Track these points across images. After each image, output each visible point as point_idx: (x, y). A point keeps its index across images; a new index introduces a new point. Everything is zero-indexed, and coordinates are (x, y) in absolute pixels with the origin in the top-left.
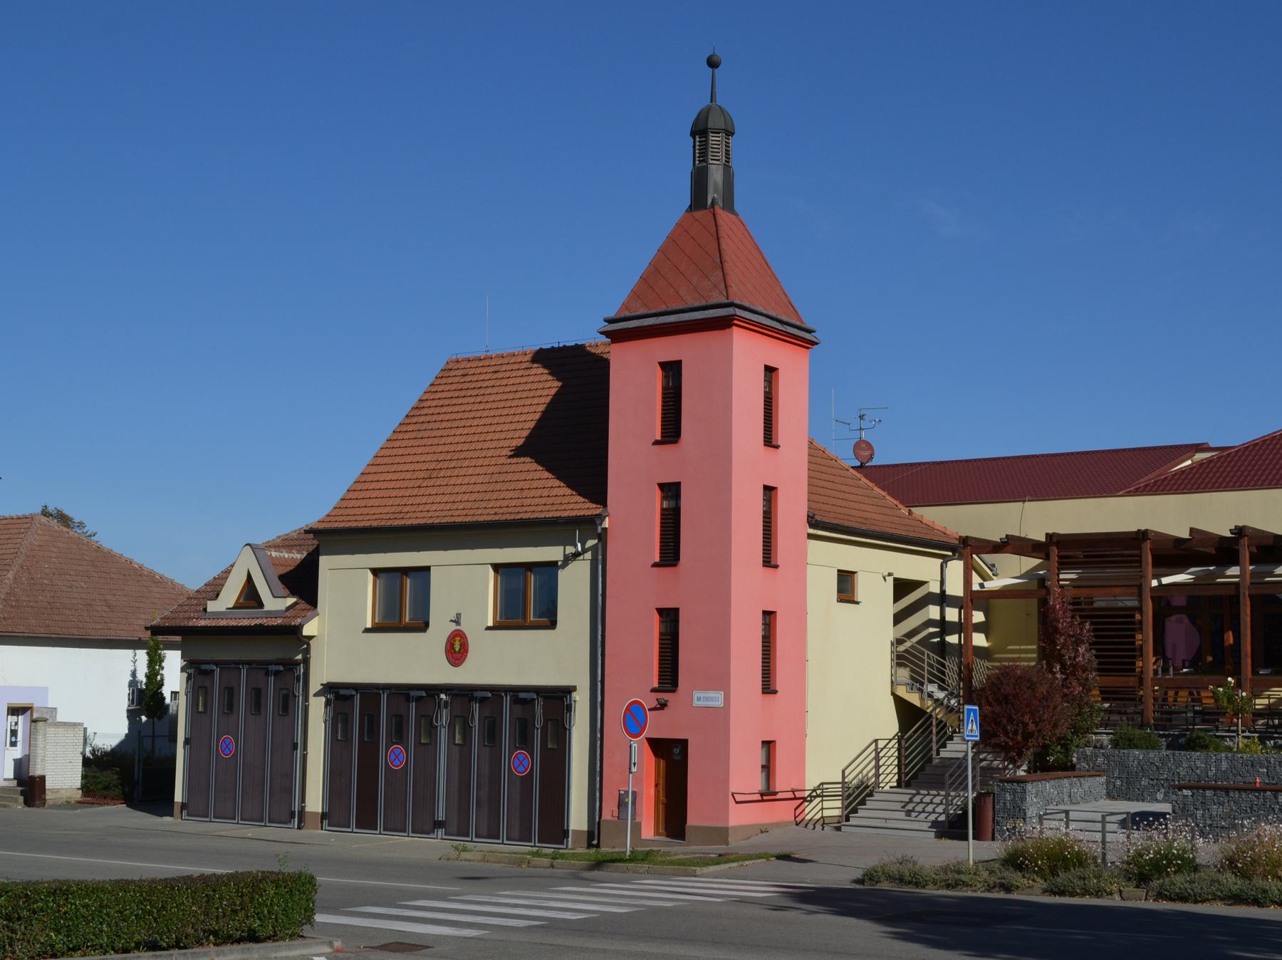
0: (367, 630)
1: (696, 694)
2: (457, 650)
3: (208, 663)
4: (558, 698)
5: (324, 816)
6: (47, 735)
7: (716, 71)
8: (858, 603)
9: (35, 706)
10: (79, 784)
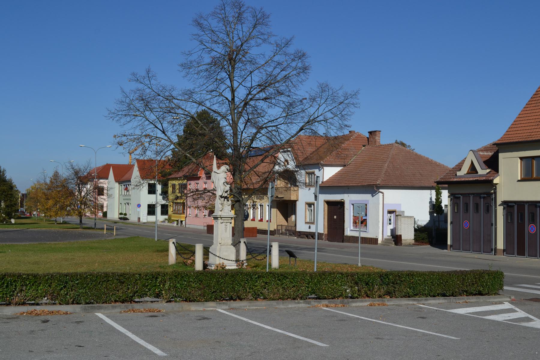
0: (519, 181)
3: (458, 194)
5: (504, 250)
9: (397, 210)
10: (413, 238)
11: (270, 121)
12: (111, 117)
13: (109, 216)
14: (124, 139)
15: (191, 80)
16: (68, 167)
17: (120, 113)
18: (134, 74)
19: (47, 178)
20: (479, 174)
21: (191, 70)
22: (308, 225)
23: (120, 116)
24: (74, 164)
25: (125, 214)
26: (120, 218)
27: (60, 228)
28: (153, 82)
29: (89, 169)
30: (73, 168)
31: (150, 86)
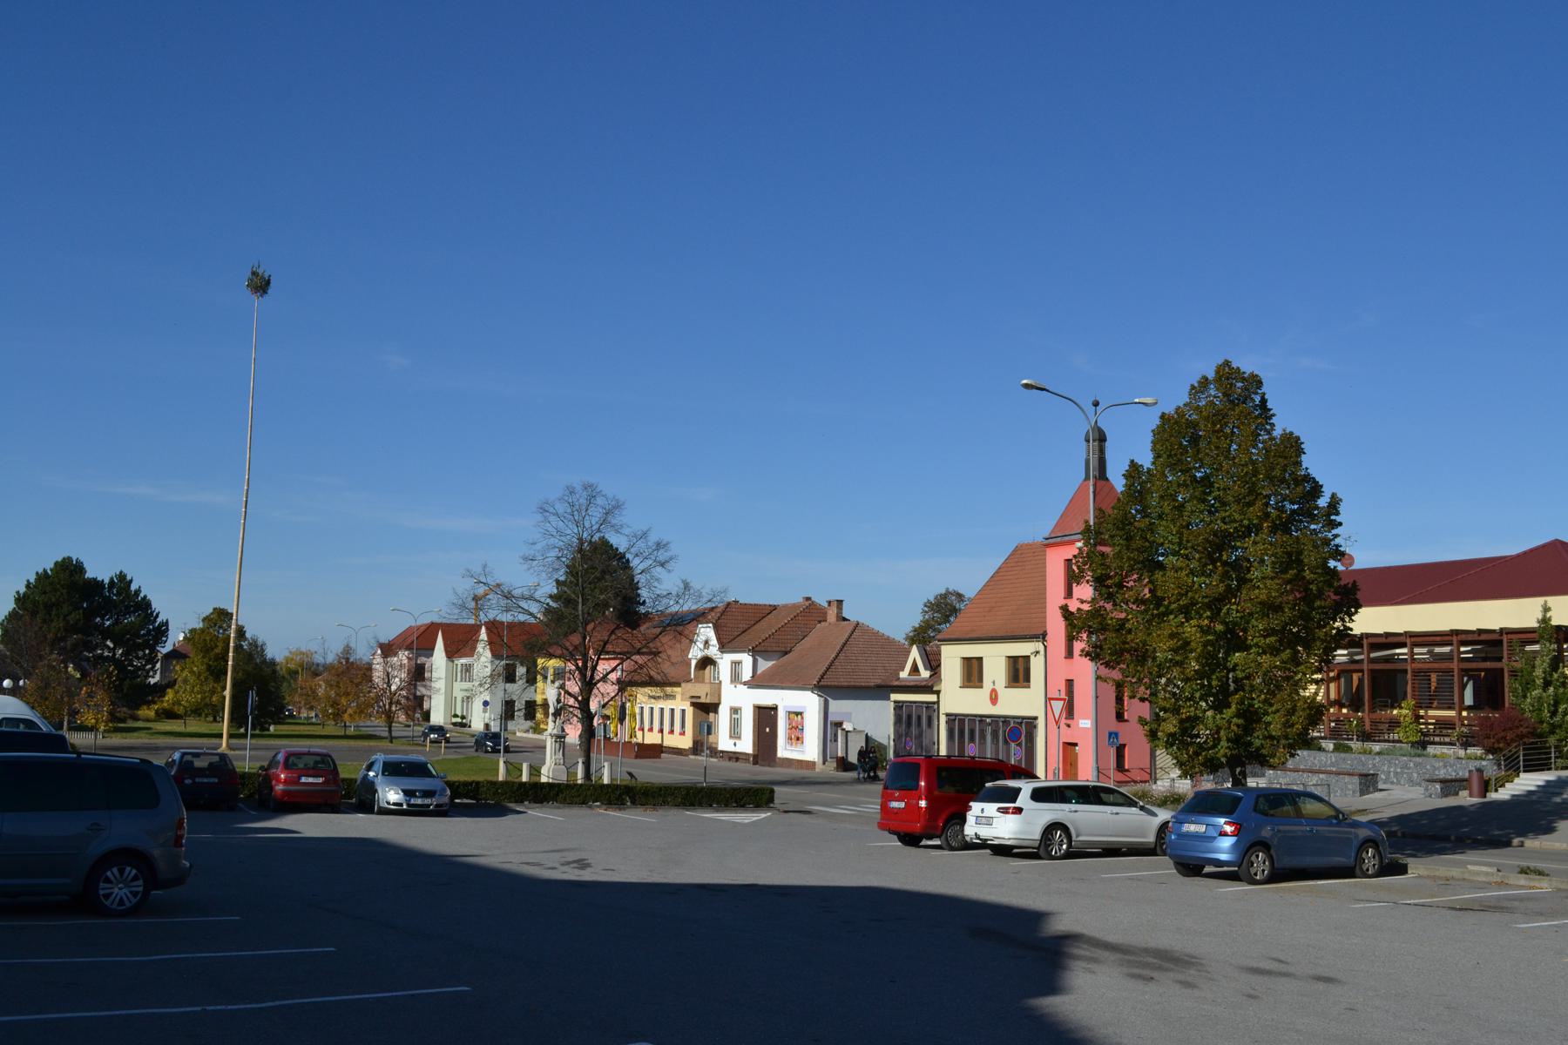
1: (1081, 721)
2: (994, 699)
4: (1030, 722)
6: (394, 724)
8: (140, 587)
22: (732, 741)
25: (463, 717)
26: (455, 724)
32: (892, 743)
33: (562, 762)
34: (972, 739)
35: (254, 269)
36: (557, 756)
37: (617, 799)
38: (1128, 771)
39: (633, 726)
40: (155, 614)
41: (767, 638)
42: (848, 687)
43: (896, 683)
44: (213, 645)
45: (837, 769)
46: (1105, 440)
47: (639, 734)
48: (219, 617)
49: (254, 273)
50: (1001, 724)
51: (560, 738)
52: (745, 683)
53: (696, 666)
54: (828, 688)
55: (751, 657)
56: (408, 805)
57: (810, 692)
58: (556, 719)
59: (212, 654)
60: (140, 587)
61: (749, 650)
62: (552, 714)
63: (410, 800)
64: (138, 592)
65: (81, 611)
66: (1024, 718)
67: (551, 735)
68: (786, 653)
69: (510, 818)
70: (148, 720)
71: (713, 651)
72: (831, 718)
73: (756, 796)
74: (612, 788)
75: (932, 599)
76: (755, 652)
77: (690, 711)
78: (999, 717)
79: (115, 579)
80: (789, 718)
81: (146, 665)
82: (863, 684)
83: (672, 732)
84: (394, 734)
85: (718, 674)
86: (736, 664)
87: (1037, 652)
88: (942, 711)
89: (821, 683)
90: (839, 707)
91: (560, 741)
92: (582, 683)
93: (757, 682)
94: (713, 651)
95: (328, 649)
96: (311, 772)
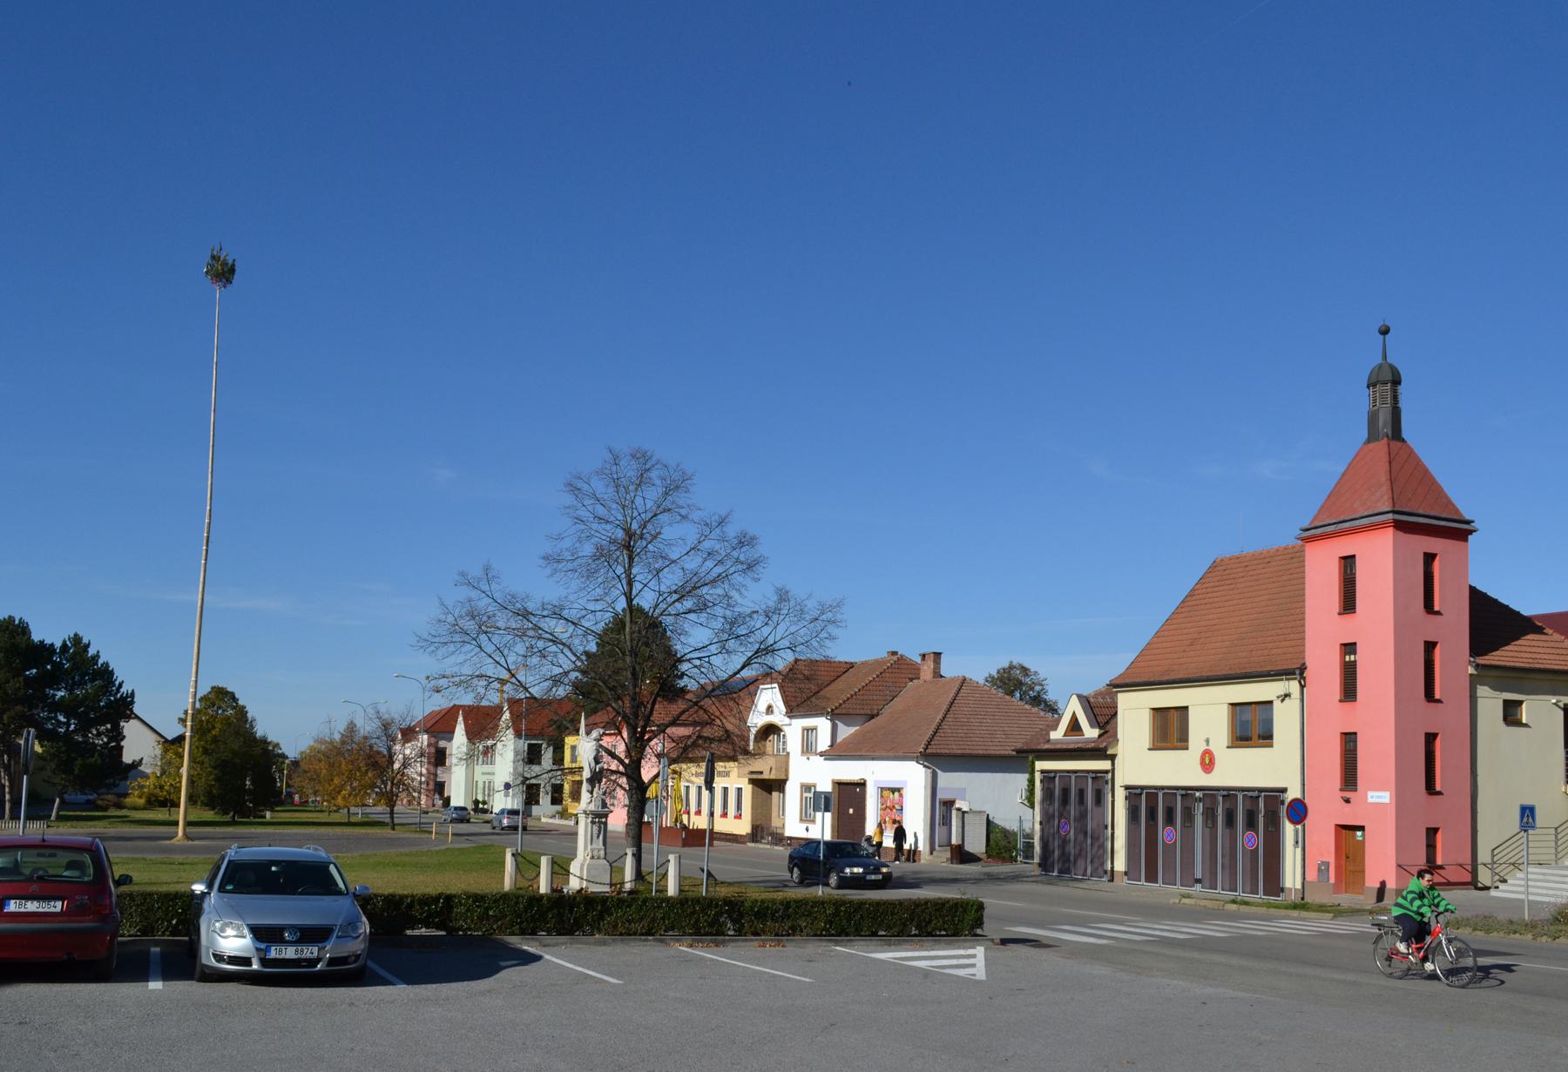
1: (1370, 794)
2: (1208, 762)
5: (1126, 873)
7: (1387, 336)
8: (98, 652)
11: (696, 650)
12: (422, 647)
13: (454, 803)
14: (443, 682)
15: (561, 583)
16: (370, 716)
17: (436, 640)
18: (463, 574)
19: (336, 732)
20: (1086, 736)
21: (560, 566)
22: (804, 825)
23: (436, 645)
24: (383, 710)
27: (39, 855)
28: (494, 586)
29: (408, 719)
30: (380, 718)
31: (489, 593)
32: (1037, 827)
33: (602, 853)
34: (1170, 819)
35: (215, 253)
36: (594, 846)
37: (711, 925)
38: (1441, 867)
39: (679, 809)
40: (117, 683)
41: (848, 699)
42: (962, 756)
43: (1046, 746)
44: (210, 726)
45: (952, 860)
46: (1399, 383)
47: (685, 817)
48: (218, 697)
49: (213, 257)
50: (1221, 799)
51: (600, 817)
52: (821, 754)
53: (756, 737)
54: (936, 758)
55: (829, 722)
56: (264, 962)
57: (914, 763)
58: (593, 787)
59: (209, 737)
60: (98, 652)
61: (828, 713)
62: (587, 780)
63: (267, 950)
64: (97, 656)
65: (21, 679)
66: (1261, 790)
67: (585, 812)
68: (872, 717)
69: (510, 976)
70: (135, 808)
71: (779, 718)
72: (940, 796)
73: (953, 917)
74: (684, 902)
75: (994, 673)
76: (835, 715)
77: (748, 790)
78: (1218, 789)
79: (68, 643)
80: (882, 797)
81: (108, 743)
82: (981, 752)
83: (725, 815)
84: (396, 821)
85: (784, 743)
86: (809, 732)
87: (1287, 695)
88: (1119, 782)
89: (928, 751)
90: (951, 781)
91: (600, 822)
92: (630, 738)
93: (836, 752)
94: (779, 718)
95: (335, 729)
96: (35, 888)
